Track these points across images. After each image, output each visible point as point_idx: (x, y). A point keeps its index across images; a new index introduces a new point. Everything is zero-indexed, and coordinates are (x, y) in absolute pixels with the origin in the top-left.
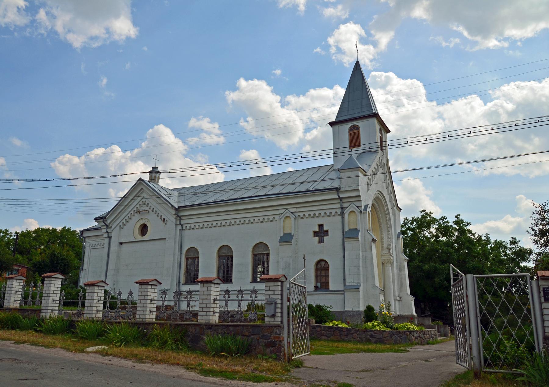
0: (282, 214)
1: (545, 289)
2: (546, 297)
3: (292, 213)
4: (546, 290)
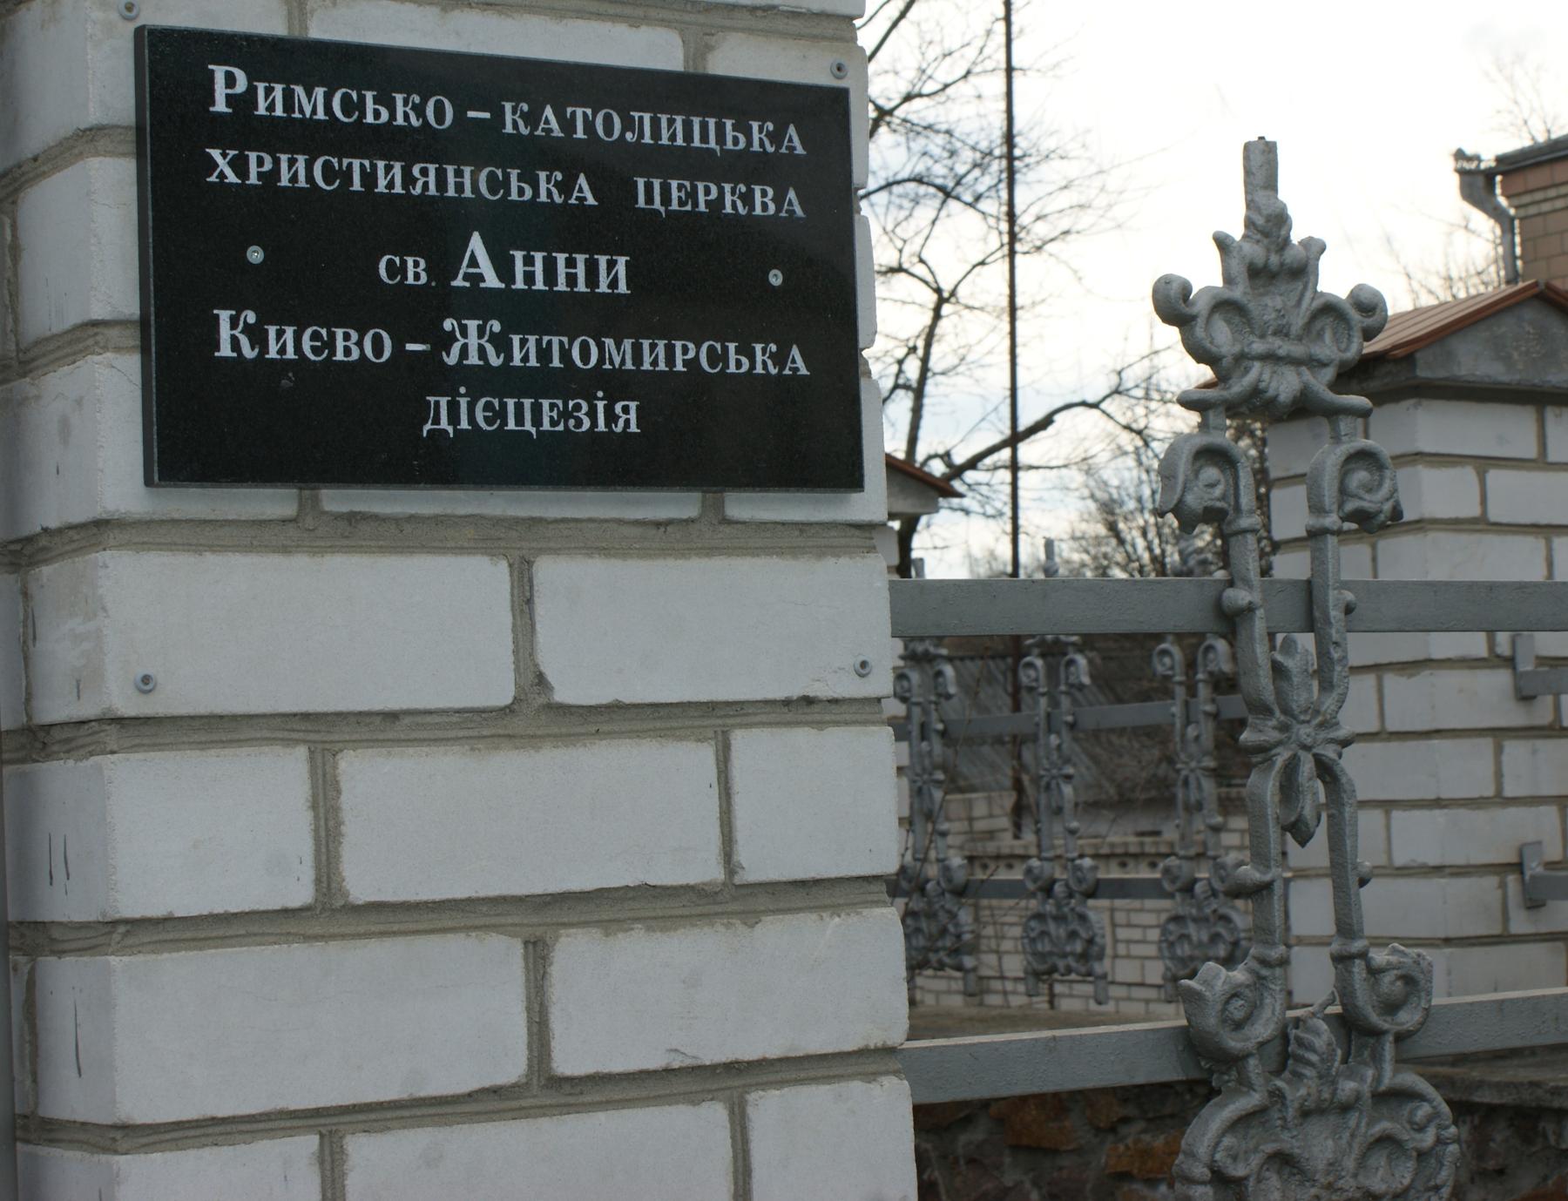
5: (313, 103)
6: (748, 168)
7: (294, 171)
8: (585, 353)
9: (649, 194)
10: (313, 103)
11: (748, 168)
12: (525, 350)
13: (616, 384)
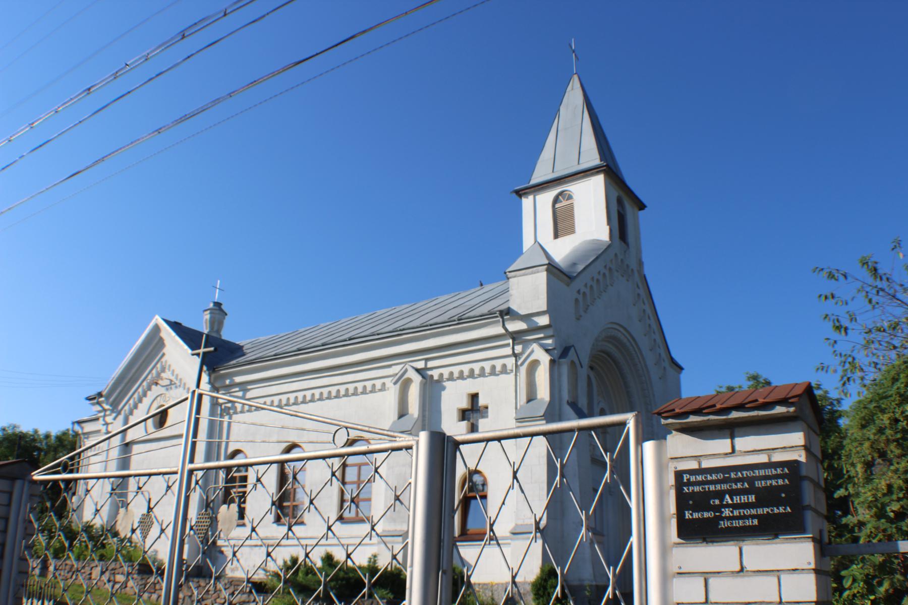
0: (397, 374)
1: (686, 477)
2: (688, 515)
3: (418, 370)
4: (689, 483)
5: (699, 478)
6: (777, 477)
7: (697, 489)
8: (747, 512)
9: (758, 484)
10: (699, 478)
11: (777, 477)
12: (736, 513)
13: (753, 517)
